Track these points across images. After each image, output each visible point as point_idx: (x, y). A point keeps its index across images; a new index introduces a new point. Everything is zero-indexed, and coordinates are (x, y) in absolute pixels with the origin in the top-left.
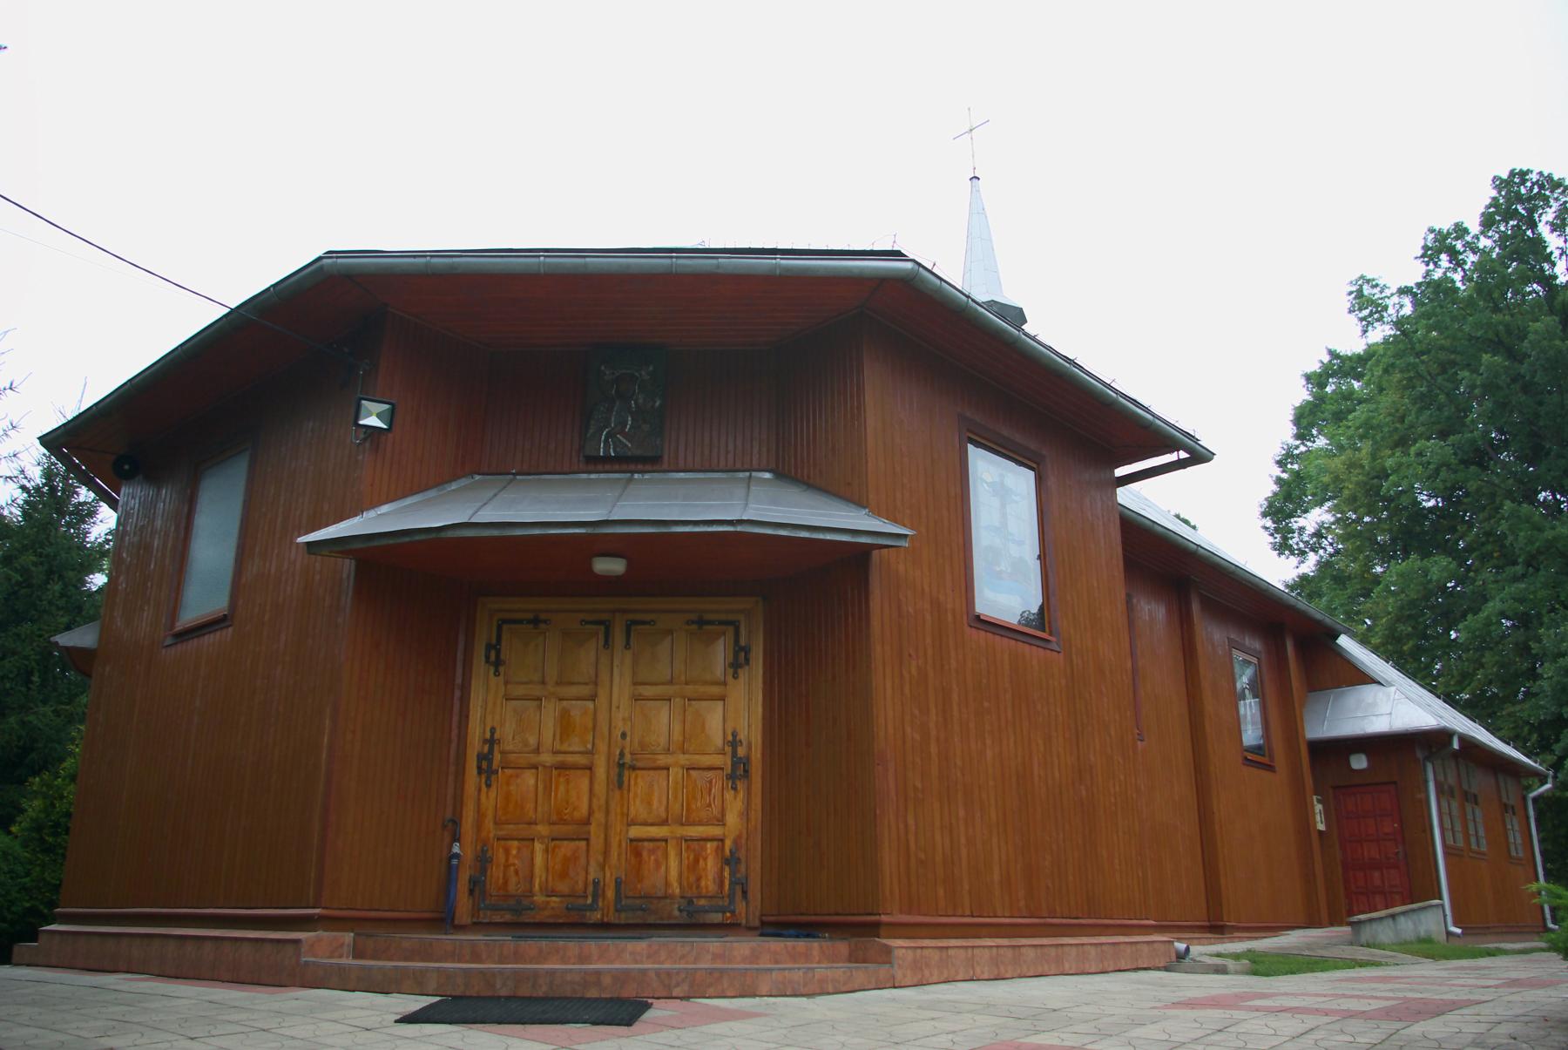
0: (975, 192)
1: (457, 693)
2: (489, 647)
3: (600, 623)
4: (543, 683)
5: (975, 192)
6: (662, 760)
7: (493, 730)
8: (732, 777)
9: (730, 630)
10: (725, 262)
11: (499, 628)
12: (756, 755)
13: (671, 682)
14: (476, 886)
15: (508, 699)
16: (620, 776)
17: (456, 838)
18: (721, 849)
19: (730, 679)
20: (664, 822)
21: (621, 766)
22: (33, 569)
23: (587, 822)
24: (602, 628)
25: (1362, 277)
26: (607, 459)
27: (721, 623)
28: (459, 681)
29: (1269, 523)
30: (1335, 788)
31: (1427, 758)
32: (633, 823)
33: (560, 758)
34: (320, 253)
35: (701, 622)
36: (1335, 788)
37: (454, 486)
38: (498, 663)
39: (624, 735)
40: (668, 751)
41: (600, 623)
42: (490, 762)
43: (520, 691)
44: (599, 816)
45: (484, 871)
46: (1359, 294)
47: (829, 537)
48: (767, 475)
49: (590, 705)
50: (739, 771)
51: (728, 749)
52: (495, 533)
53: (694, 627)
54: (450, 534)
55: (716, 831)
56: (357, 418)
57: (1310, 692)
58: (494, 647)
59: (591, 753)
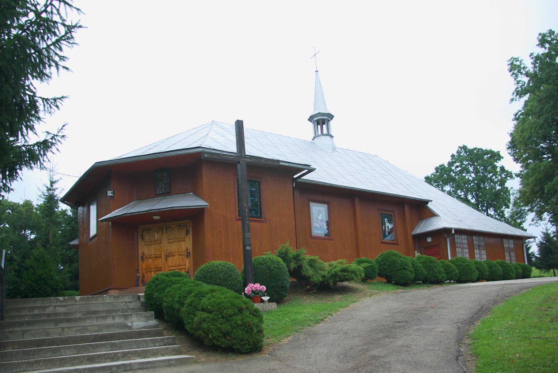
0: (317, 76)
1: (136, 245)
2: (141, 235)
3: (185, 225)
4: (151, 242)
5: (317, 76)
6: (174, 254)
7: (143, 252)
8: (187, 256)
9: (185, 227)
10: (166, 155)
11: (143, 231)
12: (191, 252)
13: (175, 239)
14: (143, 281)
15: (145, 245)
16: (166, 258)
17: (138, 273)
18: (185, 270)
19: (186, 237)
20: (175, 266)
21: (167, 256)
22: (75, 226)
23: (161, 268)
24: (161, 229)
25: (512, 58)
26: (160, 194)
27: (184, 226)
28: (136, 242)
29: (509, 151)
30: (424, 248)
31: (447, 237)
32: (169, 267)
33: (156, 256)
34: (94, 164)
35: (180, 226)
36: (424, 248)
37: (131, 204)
38: (143, 239)
39: (167, 250)
40: (175, 253)
41: (185, 225)
42: (143, 258)
43: (147, 243)
44: (163, 266)
45: (144, 278)
46: (512, 64)
47: (191, 208)
48: (192, 193)
49: (160, 245)
50: (188, 255)
51: (186, 251)
52: (130, 215)
53: (178, 227)
54: (123, 216)
55: (184, 267)
56: (107, 194)
57: (420, 220)
58: (142, 235)
59: (161, 254)
